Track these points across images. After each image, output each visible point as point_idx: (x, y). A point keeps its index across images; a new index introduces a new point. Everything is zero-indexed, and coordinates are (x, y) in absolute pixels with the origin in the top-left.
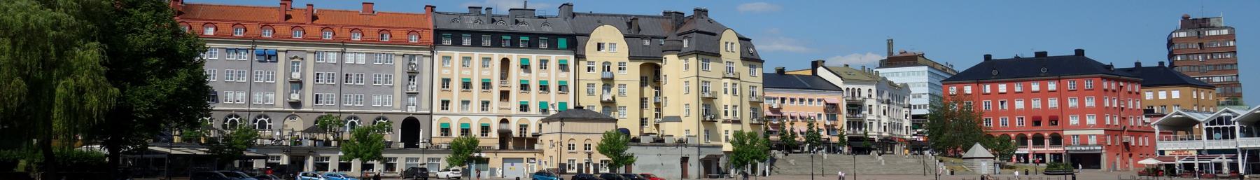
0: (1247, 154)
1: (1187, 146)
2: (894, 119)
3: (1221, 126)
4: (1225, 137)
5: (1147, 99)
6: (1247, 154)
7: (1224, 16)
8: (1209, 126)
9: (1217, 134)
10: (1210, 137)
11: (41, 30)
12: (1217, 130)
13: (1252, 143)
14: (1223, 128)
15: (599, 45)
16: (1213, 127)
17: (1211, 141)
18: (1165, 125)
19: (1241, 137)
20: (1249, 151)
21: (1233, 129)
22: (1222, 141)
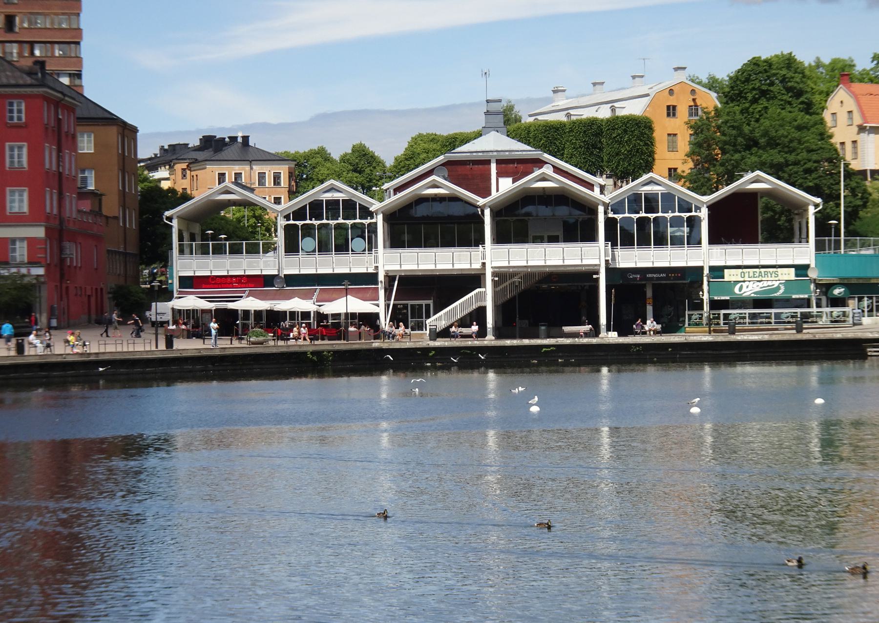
0: (396, 283)
1: (245, 267)
2: (367, 178)
3: (316, 223)
4: (323, 248)
5: (199, 144)
6: (396, 283)
7: (819, 56)
8: (292, 222)
9: (308, 240)
10: (292, 248)
11: (736, 76)
12: (308, 231)
13: (206, 267)
14: (639, 219)
15: (842, 102)
16: (300, 223)
17: (293, 258)
18: (182, 218)
19: (384, 247)
20: (401, 278)
21: (373, 228)
22: (318, 257)
